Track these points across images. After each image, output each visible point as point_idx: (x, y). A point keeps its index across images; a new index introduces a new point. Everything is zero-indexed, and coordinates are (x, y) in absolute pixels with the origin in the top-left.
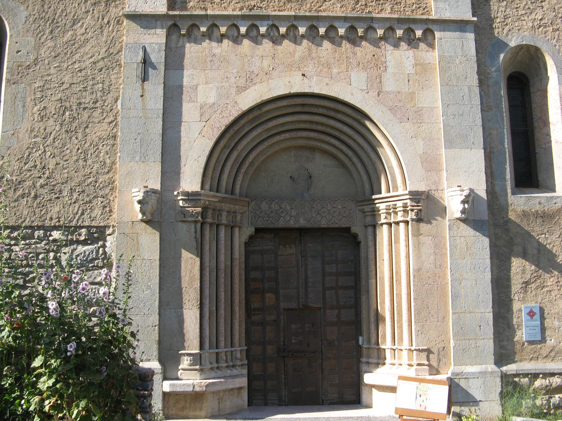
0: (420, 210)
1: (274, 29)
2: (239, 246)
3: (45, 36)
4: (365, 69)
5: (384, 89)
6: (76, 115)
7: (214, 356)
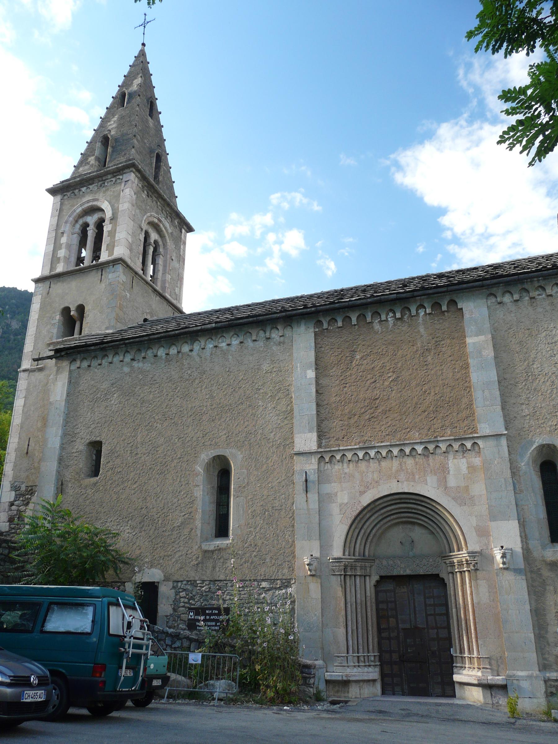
0: (477, 563)
1: (379, 454)
2: (370, 588)
3: (252, 469)
4: (435, 474)
5: (448, 486)
6: (271, 514)
7: (356, 658)
